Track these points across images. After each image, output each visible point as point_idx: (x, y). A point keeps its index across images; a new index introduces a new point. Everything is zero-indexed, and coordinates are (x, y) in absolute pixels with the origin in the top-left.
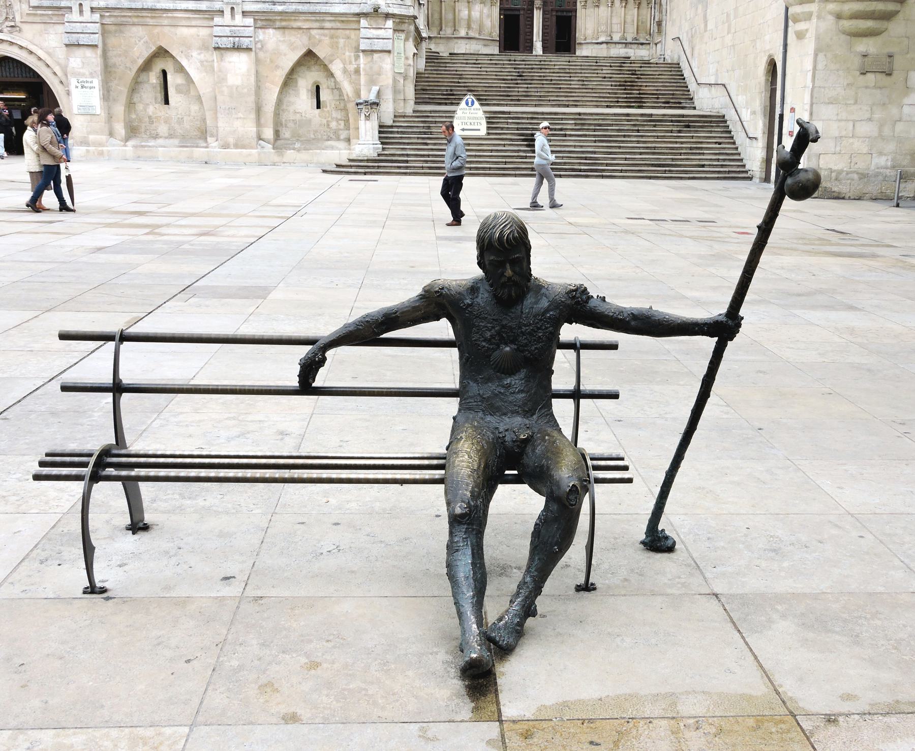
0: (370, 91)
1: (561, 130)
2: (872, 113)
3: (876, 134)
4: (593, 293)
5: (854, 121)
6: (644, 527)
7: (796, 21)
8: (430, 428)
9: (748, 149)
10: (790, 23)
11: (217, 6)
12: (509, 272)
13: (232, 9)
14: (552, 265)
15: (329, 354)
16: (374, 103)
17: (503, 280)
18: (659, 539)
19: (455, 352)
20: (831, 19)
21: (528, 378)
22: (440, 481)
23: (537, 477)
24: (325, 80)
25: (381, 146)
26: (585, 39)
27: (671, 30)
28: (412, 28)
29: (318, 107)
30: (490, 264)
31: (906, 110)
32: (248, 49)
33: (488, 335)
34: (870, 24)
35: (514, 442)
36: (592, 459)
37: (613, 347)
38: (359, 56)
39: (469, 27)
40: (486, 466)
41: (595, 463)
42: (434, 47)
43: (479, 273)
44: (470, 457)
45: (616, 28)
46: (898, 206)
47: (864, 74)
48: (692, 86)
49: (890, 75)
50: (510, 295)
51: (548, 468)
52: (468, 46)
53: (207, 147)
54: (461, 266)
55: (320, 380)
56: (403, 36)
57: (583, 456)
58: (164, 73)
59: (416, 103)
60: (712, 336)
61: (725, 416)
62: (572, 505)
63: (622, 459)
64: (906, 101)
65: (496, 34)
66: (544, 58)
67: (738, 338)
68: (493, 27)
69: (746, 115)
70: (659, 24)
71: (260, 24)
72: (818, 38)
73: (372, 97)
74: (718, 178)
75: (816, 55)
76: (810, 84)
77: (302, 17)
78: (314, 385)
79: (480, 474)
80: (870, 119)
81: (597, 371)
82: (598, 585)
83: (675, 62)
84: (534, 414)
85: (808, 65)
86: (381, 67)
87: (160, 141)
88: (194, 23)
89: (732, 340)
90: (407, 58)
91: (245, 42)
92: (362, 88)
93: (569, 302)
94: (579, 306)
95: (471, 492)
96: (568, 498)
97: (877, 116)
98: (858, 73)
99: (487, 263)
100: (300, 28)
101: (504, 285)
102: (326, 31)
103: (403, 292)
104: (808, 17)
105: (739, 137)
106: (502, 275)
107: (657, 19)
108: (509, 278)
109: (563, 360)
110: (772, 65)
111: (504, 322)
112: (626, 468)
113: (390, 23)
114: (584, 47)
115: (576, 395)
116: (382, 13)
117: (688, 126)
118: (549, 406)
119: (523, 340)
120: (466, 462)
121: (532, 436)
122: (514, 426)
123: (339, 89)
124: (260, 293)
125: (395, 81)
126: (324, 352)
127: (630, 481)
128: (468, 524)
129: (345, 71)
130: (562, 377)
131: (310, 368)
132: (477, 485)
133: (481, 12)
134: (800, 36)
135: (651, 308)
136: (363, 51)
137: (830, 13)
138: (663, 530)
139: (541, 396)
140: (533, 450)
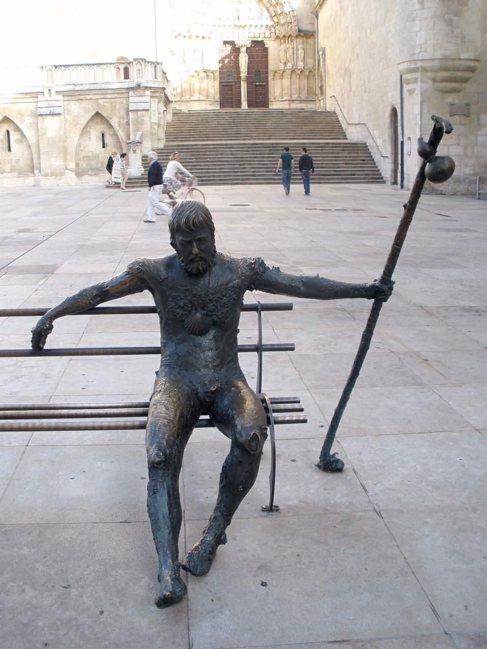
0: (136, 135)
1: (261, 154)
2: (459, 140)
3: (462, 154)
4: (269, 263)
5: (449, 145)
6: (319, 450)
7: (408, 83)
8: (140, 380)
9: (382, 164)
10: (404, 85)
11: (40, 90)
12: (196, 250)
13: (50, 90)
14: (232, 242)
15: (56, 323)
16: (138, 142)
17: (191, 257)
18: (331, 463)
19: (155, 317)
20: (430, 82)
21: (215, 339)
22: (142, 426)
23: (222, 421)
24: (108, 130)
25: (143, 169)
26: (275, 99)
27: (329, 92)
28: (163, 95)
29: (104, 147)
30: (180, 243)
31: (480, 138)
32: (60, 114)
33: (181, 304)
34: (454, 85)
35: (205, 393)
36: (272, 403)
37: (288, 307)
38: (129, 114)
39: (200, 94)
40: (182, 416)
41: (276, 406)
42: (177, 107)
43: (173, 252)
44: (167, 409)
45: (294, 91)
46: (479, 199)
47: (452, 116)
48: (344, 126)
49: (468, 116)
50: (198, 270)
51: (233, 418)
52: (200, 106)
53: (34, 176)
54: (159, 247)
55: (51, 342)
56: (156, 100)
57: (264, 401)
58: (8, 132)
59: (166, 141)
60: (369, 298)
61: (378, 351)
62: (253, 451)
63: (298, 402)
64: (480, 133)
65: (217, 97)
66: (249, 111)
67: (391, 300)
68: (215, 93)
69: (380, 142)
70: (321, 88)
71: (66, 98)
72: (422, 94)
73: (137, 139)
74: (364, 183)
75: (421, 104)
76: (419, 123)
77: (93, 92)
78: (45, 348)
79: (176, 423)
80: (458, 145)
81: (275, 328)
82: (281, 507)
83: (333, 111)
84: (222, 368)
85: (417, 110)
86: (143, 120)
87: (6, 175)
88: (26, 100)
89: (385, 301)
90: (159, 113)
91: (57, 110)
92: (131, 133)
93: (248, 273)
94: (259, 277)
95: (167, 441)
96: (249, 444)
97: (462, 142)
98: (449, 115)
99: (178, 243)
100: (91, 99)
101: (192, 261)
102: (108, 100)
103: (111, 270)
104: (415, 81)
105: (376, 157)
106: (191, 252)
107: (319, 86)
108: (196, 255)
109: (246, 321)
110: (394, 112)
111: (194, 292)
112: (301, 410)
113: (148, 93)
114: (274, 103)
115: (259, 349)
116: (143, 87)
117: (343, 150)
118: (235, 360)
119: (211, 306)
120: (163, 411)
121: (221, 388)
122: (206, 377)
123: (116, 135)
124: (48, 271)
125: (152, 127)
126: (51, 321)
127: (305, 421)
128: (165, 469)
129: (120, 124)
130: (247, 329)
131: (40, 336)
132: (173, 435)
133: (208, 84)
134: (411, 92)
135: (318, 275)
136: (131, 111)
137: (429, 78)
138: (334, 455)
139: (229, 350)
140: (222, 401)
